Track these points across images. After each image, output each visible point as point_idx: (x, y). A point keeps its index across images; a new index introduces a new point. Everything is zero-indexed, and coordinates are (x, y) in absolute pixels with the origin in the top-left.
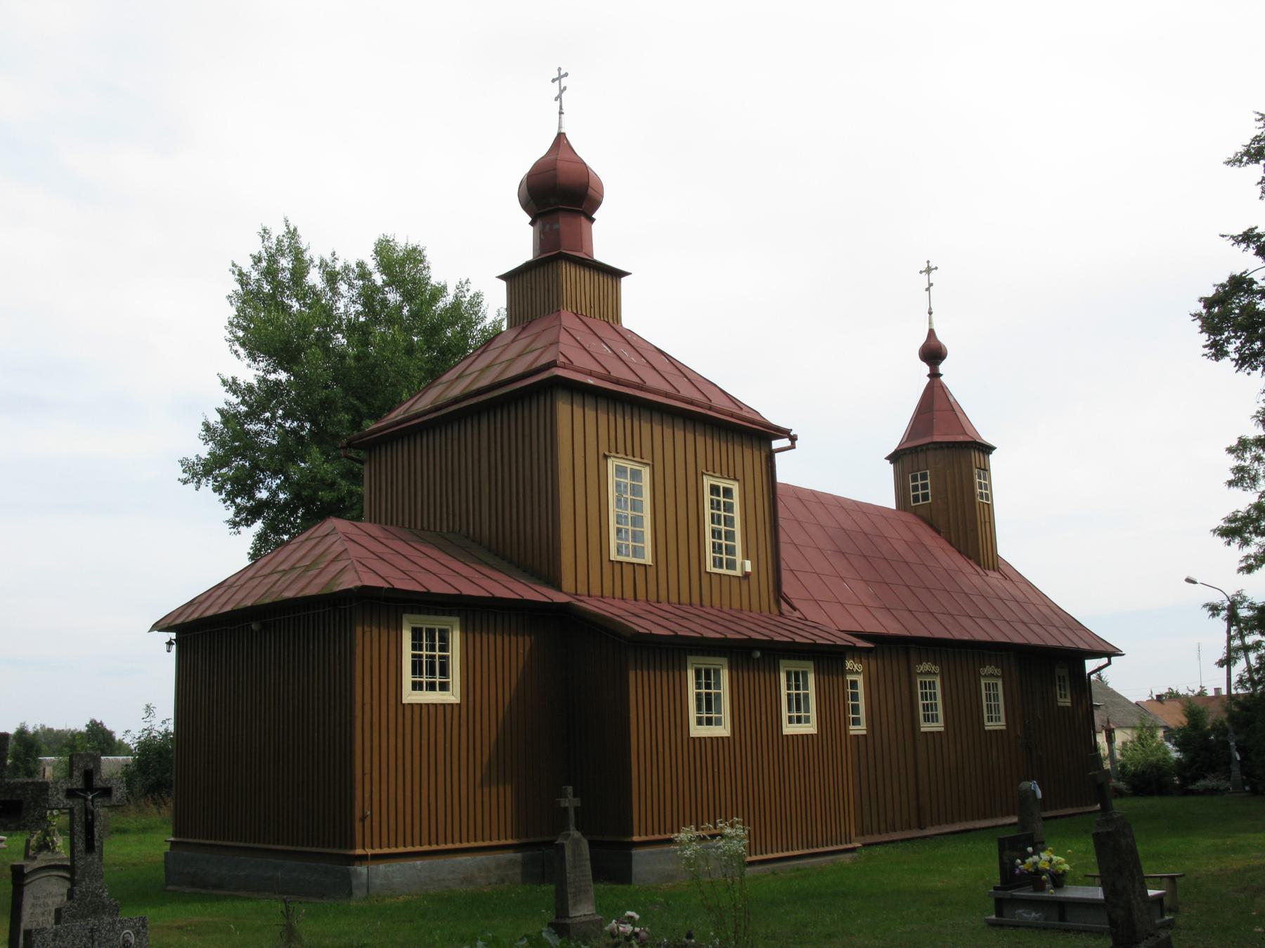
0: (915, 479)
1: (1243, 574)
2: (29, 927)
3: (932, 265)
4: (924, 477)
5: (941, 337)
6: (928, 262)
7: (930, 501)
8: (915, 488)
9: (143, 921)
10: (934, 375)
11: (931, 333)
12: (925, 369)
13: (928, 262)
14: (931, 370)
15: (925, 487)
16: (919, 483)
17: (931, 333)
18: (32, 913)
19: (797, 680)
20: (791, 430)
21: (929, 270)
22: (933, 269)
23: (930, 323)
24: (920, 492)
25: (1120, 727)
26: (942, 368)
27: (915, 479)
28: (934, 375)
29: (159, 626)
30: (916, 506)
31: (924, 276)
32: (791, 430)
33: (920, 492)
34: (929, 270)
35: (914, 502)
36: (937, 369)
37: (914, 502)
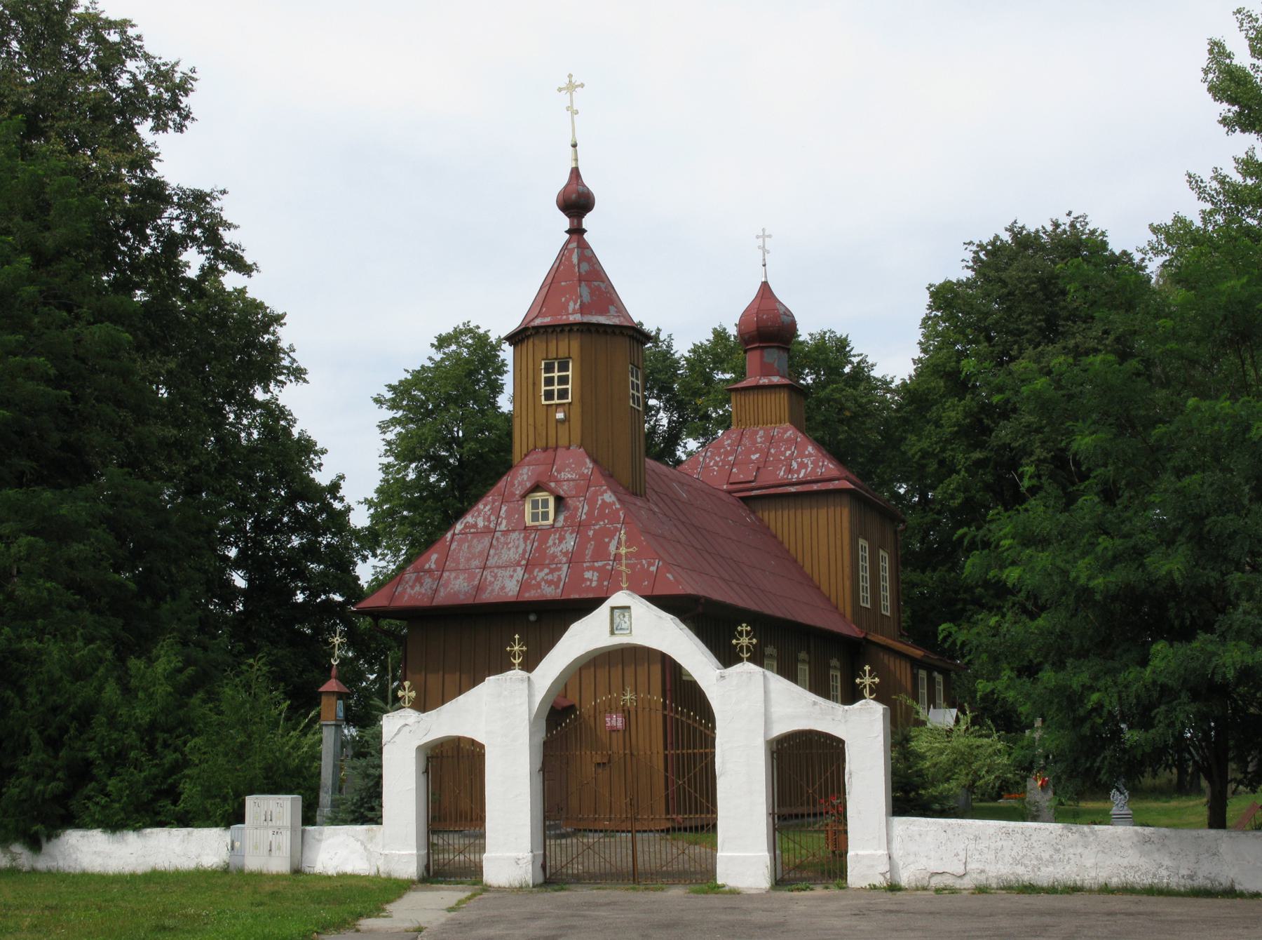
0: (549, 368)
1: (384, 427)
3: (577, 80)
4: (563, 367)
5: (589, 181)
6: (570, 76)
7: (570, 400)
8: (549, 381)
10: (576, 232)
11: (575, 173)
12: (564, 222)
13: (570, 76)
14: (571, 223)
15: (563, 380)
16: (556, 374)
17: (575, 173)
18: (94, 566)
19: (610, 706)
20: (298, 374)
21: (571, 87)
22: (571, 94)
23: (576, 151)
24: (556, 387)
26: (588, 221)
27: (549, 368)
28: (576, 232)
29: (305, 381)
30: (548, 405)
31: (565, 96)
32: (298, 374)
33: (556, 387)
34: (571, 87)
36: (580, 223)
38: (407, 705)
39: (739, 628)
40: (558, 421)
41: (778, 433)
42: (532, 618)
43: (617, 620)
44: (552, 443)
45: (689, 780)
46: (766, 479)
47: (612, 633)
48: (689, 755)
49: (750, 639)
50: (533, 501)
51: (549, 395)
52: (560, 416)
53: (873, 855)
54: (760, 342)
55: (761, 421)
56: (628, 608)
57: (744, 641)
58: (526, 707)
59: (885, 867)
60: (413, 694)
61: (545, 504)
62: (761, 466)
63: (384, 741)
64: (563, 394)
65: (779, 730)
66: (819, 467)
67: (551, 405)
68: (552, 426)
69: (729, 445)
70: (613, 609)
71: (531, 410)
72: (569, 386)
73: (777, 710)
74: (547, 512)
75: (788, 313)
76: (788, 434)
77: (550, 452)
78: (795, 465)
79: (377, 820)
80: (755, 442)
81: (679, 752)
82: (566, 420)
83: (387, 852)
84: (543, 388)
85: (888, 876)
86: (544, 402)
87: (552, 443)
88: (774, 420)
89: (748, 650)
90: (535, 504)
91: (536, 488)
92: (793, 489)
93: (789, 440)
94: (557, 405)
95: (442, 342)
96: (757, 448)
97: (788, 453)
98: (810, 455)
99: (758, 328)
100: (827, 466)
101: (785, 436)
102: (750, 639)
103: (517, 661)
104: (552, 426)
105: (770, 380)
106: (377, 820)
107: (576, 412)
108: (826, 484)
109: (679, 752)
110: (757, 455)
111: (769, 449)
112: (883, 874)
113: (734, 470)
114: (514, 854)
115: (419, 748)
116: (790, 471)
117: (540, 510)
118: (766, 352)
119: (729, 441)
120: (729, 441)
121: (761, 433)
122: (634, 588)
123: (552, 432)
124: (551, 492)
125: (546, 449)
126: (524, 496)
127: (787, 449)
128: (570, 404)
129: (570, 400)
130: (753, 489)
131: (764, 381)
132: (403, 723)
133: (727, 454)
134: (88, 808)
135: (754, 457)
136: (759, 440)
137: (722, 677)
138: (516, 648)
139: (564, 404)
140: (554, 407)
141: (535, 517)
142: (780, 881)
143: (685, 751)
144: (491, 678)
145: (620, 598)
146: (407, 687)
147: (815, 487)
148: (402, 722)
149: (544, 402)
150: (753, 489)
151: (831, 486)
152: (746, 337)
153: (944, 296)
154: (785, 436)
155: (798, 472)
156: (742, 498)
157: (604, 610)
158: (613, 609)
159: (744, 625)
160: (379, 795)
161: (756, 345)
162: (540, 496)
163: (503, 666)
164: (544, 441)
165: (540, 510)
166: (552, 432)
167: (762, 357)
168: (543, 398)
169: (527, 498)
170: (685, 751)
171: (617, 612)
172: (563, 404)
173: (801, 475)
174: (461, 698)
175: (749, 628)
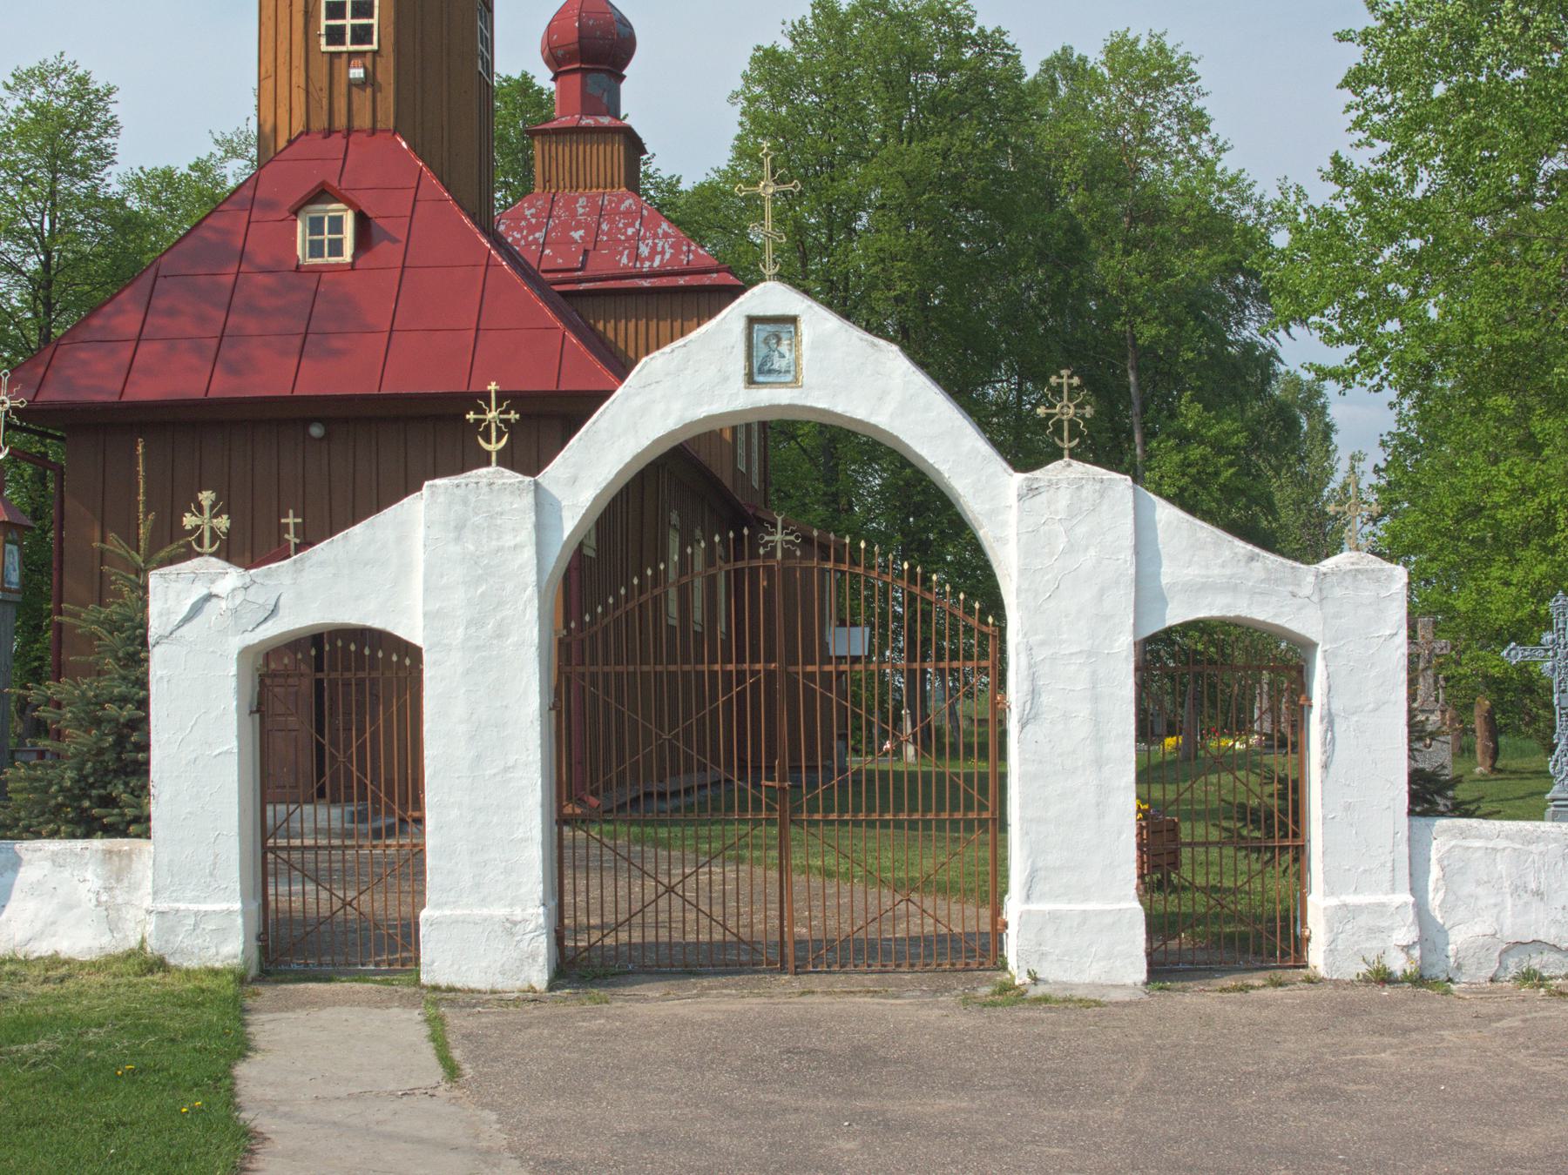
0: (336, 11)
2: (803, 327)
9: (1538, 893)
25: (530, 997)
27: (336, 11)
30: (331, 54)
35: (328, 44)
37: (328, 44)
38: (207, 548)
39: (1053, 380)
40: (351, 84)
41: (610, 202)
42: (316, 431)
43: (760, 351)
44: (341, 122)
45: (687, 730)
46: (596, 266)
47: (751, 381)
48: (686, 674)
49: (1080, 406)
50: (312, 219)
51: (335, 35)
52: (357, 73)
53: (1383, 905)
54: (582, 62)
55: (581, 183)
56: (793, 320)
57: (1066, 411)
58: (529, 554)
59: (1406, 933)
60: (223, 523)
61: (337, 224)
62: (590, 247)
63: (154, 632)
64: (362, 34)
65: (1175, 615)
66: (681, 252)
67: (340, 53)
68: (341, 89)
69: (533, 215)
70: (752, 321)
71: (299, 61)
72: (375, 21)
73: (1169, 574)
74: (340, 242)
75: (628, 26)
76: (627, 203)
77: (337, 141)
78: (644, 251)
79: (136, 824)
80: (573, 214)
81: (732, 667)
82: (370, 81)
83: (163, 906)
84: (324, 23)
85: (1416, 953)
86: (324, 48)
87: (341, 122)
88: (594, 184)
89: (1074, 432)
90: (316, 225)
91: (322, 194)
92: (646, 283)
93: (627, 213)
94: (350, 54)
95: (22, 80)
96: (579, 222)
97: (630, 231)
98: (666, 235)
99: (580, 37)
100: (695, 252)
101: (623, 208)
102: (1080, 406)
103: (493, 447)
104: (341, 89)
105: (596, 121)
106: (136, 824)
107: (386, 74)
108: (699, 277)
109: (732, 667)
110: (581, 232)
111: (599, 225)
112: (1406, 949)
113: (547, 251)
114: (500, 911)
115: (245, 653)
116: (636, 256)
117: (327, 236)
118: (591, 78)
119: (533, 211)
120: (533, 211)
121: (582, 201)
122: (794, 278)
123: (341, 105)
124: (351, 204)
125: (329, 132)
126: (296, 213)
127: (626, 226)
128: (374, 53)
129: (375, 46)
130: (580, 281)
131: (588, 121)
132: (205, 592)
133: (533, 229)
134: (1392, 84)
135: (577, 235)
136: (581, 211)
137: (1032, 491)
138: (492, 415)
139: (364, 53)
140: (345, 57)
141: (316, 249)
142: (1161, 968)
143: (717, 667)
144: (438, 482)
145: (770, 297)
146: (206, 503)
147: (681, 281)
148: (200, 591)
149: (324, 48)
150: (580, 281)
151: (706, 280)
152: (560, 53)
153: (768, 60)
154: (623, 208)
155: (651, 258)
156: (564, 294)
157: (731, 318)
158: (752, 321)
159: (1064, 372)
160: (140, 769)
161: (576, 66)
162: (335, 208)
163: (467, 459)
164: (325, 118)
165: (327, 236)
166: (341, 105)
167: (584, 85)
168: (323, 40)
169: (302, 214)
170: (717, 667)
171: (761, 331)
172: (363, 54)
173: (657, 263)
174: (358, 530)
175: (1076, 381)
